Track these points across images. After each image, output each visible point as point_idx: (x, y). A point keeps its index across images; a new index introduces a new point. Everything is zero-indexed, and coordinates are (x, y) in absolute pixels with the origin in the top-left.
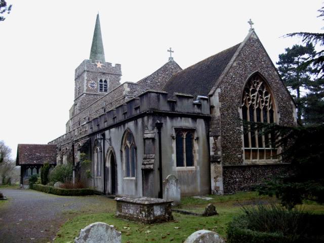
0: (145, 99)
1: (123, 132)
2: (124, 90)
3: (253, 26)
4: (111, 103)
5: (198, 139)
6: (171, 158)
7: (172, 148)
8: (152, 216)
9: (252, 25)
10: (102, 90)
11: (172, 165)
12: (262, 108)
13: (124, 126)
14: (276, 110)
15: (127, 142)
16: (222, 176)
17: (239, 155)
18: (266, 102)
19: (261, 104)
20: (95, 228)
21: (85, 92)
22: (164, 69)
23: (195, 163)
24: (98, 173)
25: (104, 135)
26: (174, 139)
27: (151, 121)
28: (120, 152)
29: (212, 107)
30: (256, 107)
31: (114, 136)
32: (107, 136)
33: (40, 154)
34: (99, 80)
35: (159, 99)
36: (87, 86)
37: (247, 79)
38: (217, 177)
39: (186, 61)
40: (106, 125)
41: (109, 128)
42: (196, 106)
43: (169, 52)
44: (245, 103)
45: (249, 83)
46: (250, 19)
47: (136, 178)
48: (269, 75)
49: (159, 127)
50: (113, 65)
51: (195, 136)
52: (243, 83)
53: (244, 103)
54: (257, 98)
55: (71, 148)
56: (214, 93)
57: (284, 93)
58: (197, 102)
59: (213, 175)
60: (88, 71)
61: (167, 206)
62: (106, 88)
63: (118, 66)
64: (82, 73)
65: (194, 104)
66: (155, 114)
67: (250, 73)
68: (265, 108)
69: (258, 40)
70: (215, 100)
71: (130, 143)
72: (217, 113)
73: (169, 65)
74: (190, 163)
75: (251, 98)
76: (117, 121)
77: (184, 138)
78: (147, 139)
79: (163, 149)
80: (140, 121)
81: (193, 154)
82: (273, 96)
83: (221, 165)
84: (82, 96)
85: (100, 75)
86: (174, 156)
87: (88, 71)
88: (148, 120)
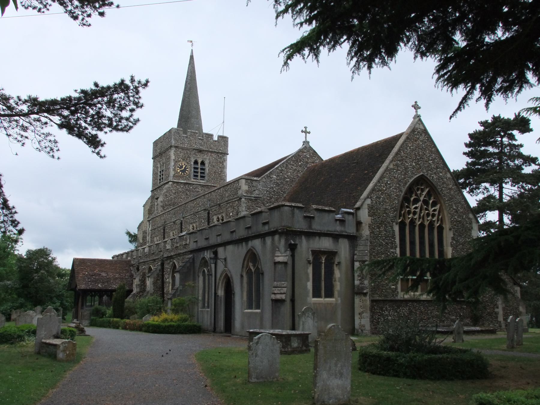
0: (276, 213)
2: (240, 189)
3: (420, 112)
4: (219, 205)
5: (339, 263)
6: (307, 286)
7: (307, 274)
8: (289, 347)
9: (419, 110)
12: (427, 223)
13: (247, 244)
14: (447, 226)
15: (251, 264)
16: (369, 312)
17: (393, 285)
18: (433, 215)
20: (264, 337)
21: (171, 179)
22: (298, 157)
23: (336, 293)
24: (204, 304)
25: (216, 253)
26: (310, 263)
27: (283, 241)
28: (239, 276)
29: (359, 224)
31: (232, 259)
33: (107, 273)
34: (193, 160)
35: (293, 214)
36: (174, 170)
38: (363, 312)
39: (327, 150)
40: (219, 240)
41: (225, 244)
42: (338, 222)
43: (308, 131)
44: (404, 216)
45: (410, 190)
46: (416, 102)
47: (262, 312)
49: (292, 248)
51: (337, 260)
52: (401, 191)
53: (402, 218)
54: (421, 210)
55: (160, 267)
56: (362, 205)
57: (460, 203)
58: (339, 216)
59: (357, 310)
60: (176, 147)
61: (304, 338)
62: (204, 173)
63: (224, 140)
65: (336, 220)
66: (289, 233)
68: (431, 224)
69: (425, 131)
70: (364, 215)
71: (254, 266)
72: (366, 232)
74: (329, 294)
75: (413, 210)
76: (236, 236)
77: (324, 262)
80: (269, 240)
81: (334, 283)
82: (444, 208)
83: (368, 297)
84: (167, 186)
85: (195, 154)
86: (310, 285)
87: (176, 147)
88: (280, 240)
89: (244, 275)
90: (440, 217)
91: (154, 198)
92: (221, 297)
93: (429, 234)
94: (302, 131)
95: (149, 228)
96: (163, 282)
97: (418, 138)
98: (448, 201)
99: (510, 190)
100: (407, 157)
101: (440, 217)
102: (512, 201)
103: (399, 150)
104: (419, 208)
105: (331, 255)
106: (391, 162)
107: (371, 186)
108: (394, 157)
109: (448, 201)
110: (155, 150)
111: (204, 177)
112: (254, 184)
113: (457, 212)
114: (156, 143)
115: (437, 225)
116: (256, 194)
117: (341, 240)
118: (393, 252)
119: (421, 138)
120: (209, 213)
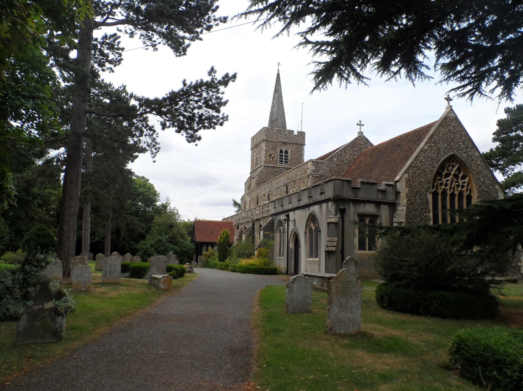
1: (308, 215)
4: (294, 181)
9: (450, 102)
10: (282, 161)
11: (355, 249)
12: (457, 193)
13: (309, 209)
15: (312, 225)
18: (463, 187)
19: (456, 188)
22: (354, 144)
25: (288, 216)
29: (398, 193)
30: (449, 192)
31: (299, 219)
32: (292, 217)
34: (279, 150)
36: (265, 157)
37: (440, 163)
40: (290, 207)
44: (437, 187)
45: (442, 166)
47: (320, 259)
48: (468, 156)
49: (342, 212)
50: (296, 133)
52: (435, 167)
53: (435, 189)
60: (267, 141)
62: (287, 159)
63: (302, 134)
64: (261, 143)
65: (379, 190)
67: (443, 156)
68: (461, 194)
69: (456, 119)
71: (314, 225)
73: (358, 140)
76: (302, 203)
78: (331, 223)
79: (346, 233)
80: (324, 205)
84: (260, 169)
86: (356, 241)
87: (267, 141)
89: (307, 232)
90: (469, 188)
91: (251, 178)
92: (292, 249)
93: (459, 202)
94: (358, 124)
95: (248, 200)
96: (254, 237)
97: (450, 125)
98: (476, 174)
99: (139, 113)
100: (439, 140)
101: (469, 188)
102: (131, 118)
103: (433, 135)
104: (450, 180)
105: (374, 217)
106: (426, 144)
107: (409, 163)
108: (428, 140)
109: (476, 174)
110: (252, 144)
111: (287, 162)
112: (320, 165)
113: (484, 183)
114: (253, 138)
115: (466, 194)
116: (320, 172)
117: (383, 206)
118: (426, 216)
119: (452, 124)
120: (287, 188)
